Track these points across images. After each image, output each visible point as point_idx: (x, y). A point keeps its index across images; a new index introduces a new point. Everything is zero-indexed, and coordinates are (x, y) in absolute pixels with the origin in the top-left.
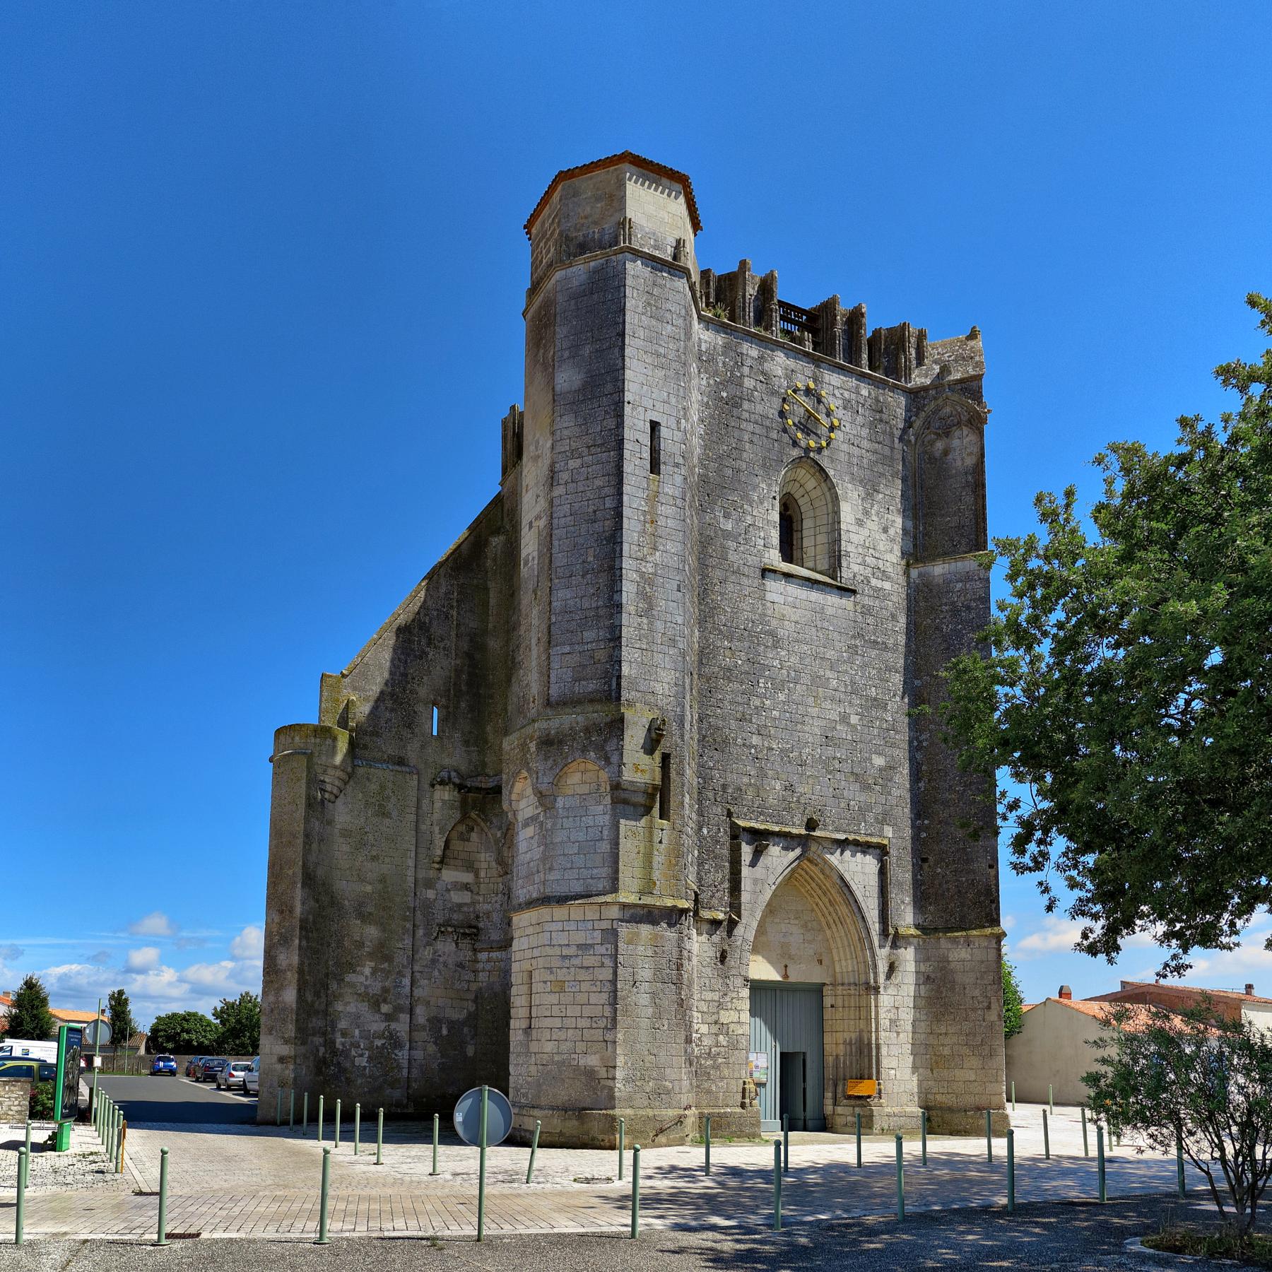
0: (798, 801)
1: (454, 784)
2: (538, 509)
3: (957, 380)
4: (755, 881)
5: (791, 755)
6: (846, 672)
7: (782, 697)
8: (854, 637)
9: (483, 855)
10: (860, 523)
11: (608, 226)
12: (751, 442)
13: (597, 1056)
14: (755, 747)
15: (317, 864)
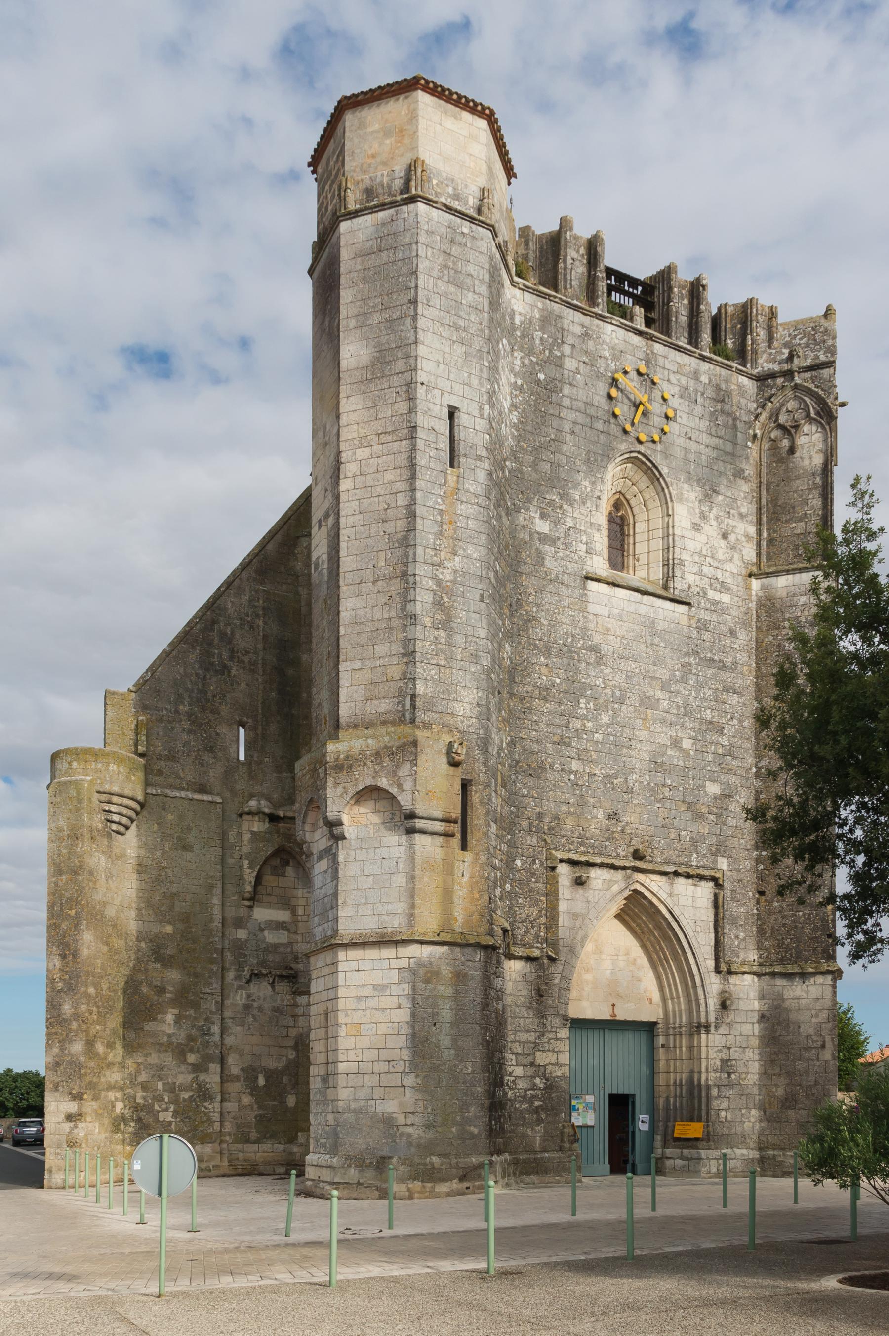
0: (623, 831)
1: (264, 814)
2: (327, 504)
5: (615, 781)
8: (687, 654)
9: (300, 891)
10: (696, 527)
12: (573, 432)
13: (396, 1102)
14: (575, 773)
15: (105, 904)
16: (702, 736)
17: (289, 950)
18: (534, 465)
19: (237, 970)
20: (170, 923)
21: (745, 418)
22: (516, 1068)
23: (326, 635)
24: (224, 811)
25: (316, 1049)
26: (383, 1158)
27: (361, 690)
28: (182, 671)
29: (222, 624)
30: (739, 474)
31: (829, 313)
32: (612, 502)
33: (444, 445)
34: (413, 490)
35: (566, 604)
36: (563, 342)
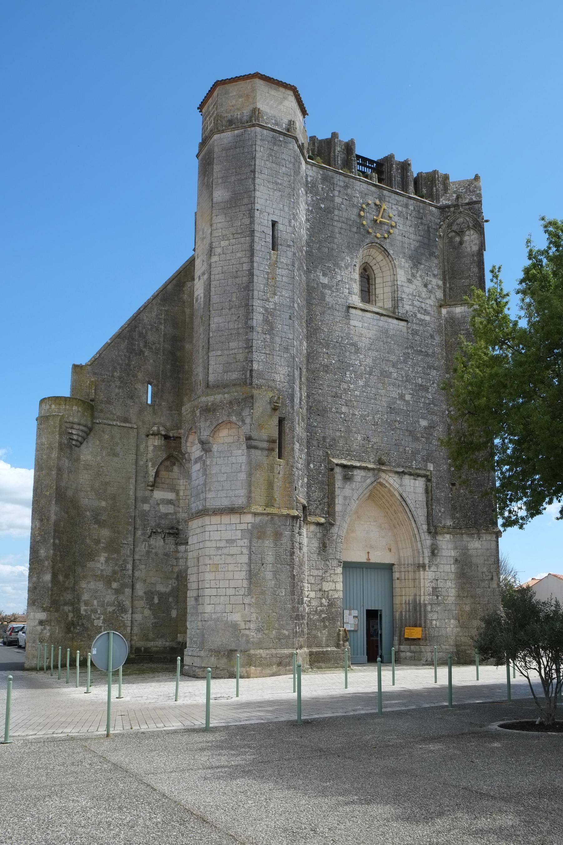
0: (372, 447)
1: (162, 435)
2: (203, 268)
3: (466, 203)
4: (345, 498)
5: (367, 419)
6: (402, 369)
7: (361, 383)
8: (407, 348)
9: (182, 481)
10: (410, 281)
11: (246, 112)
13: (239, 614)
16: (416, 393)
17: (174, 517)
18: (319, 249)
19: (143, 530)
20: (104, 500)
21: (434, 227)
22: (311, 592)
23: (202, 336)
24: (138, 433)
25: (191, 580)
26: (231, 651)
27: (221, 367)
28: (116, 353)
29: (140, 328)
30: (432, 254)
31: (477, 178)
32: (362, 267)
33: (269, 240)
34: (252, 262)
35: (338, 321)
36: (334, 190)
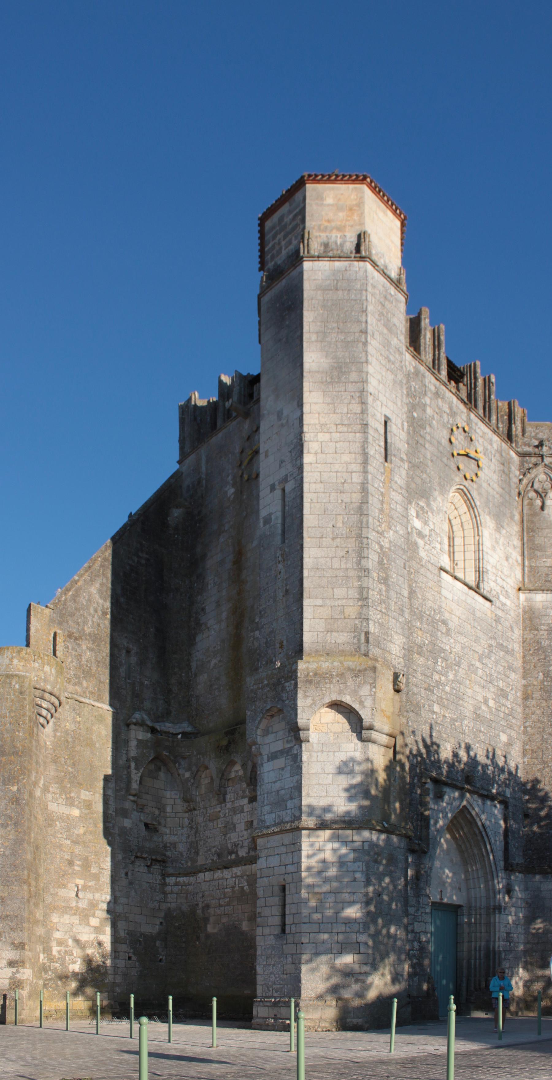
1: (148, 726)
8: (491, 638)
34: (365, 472)
